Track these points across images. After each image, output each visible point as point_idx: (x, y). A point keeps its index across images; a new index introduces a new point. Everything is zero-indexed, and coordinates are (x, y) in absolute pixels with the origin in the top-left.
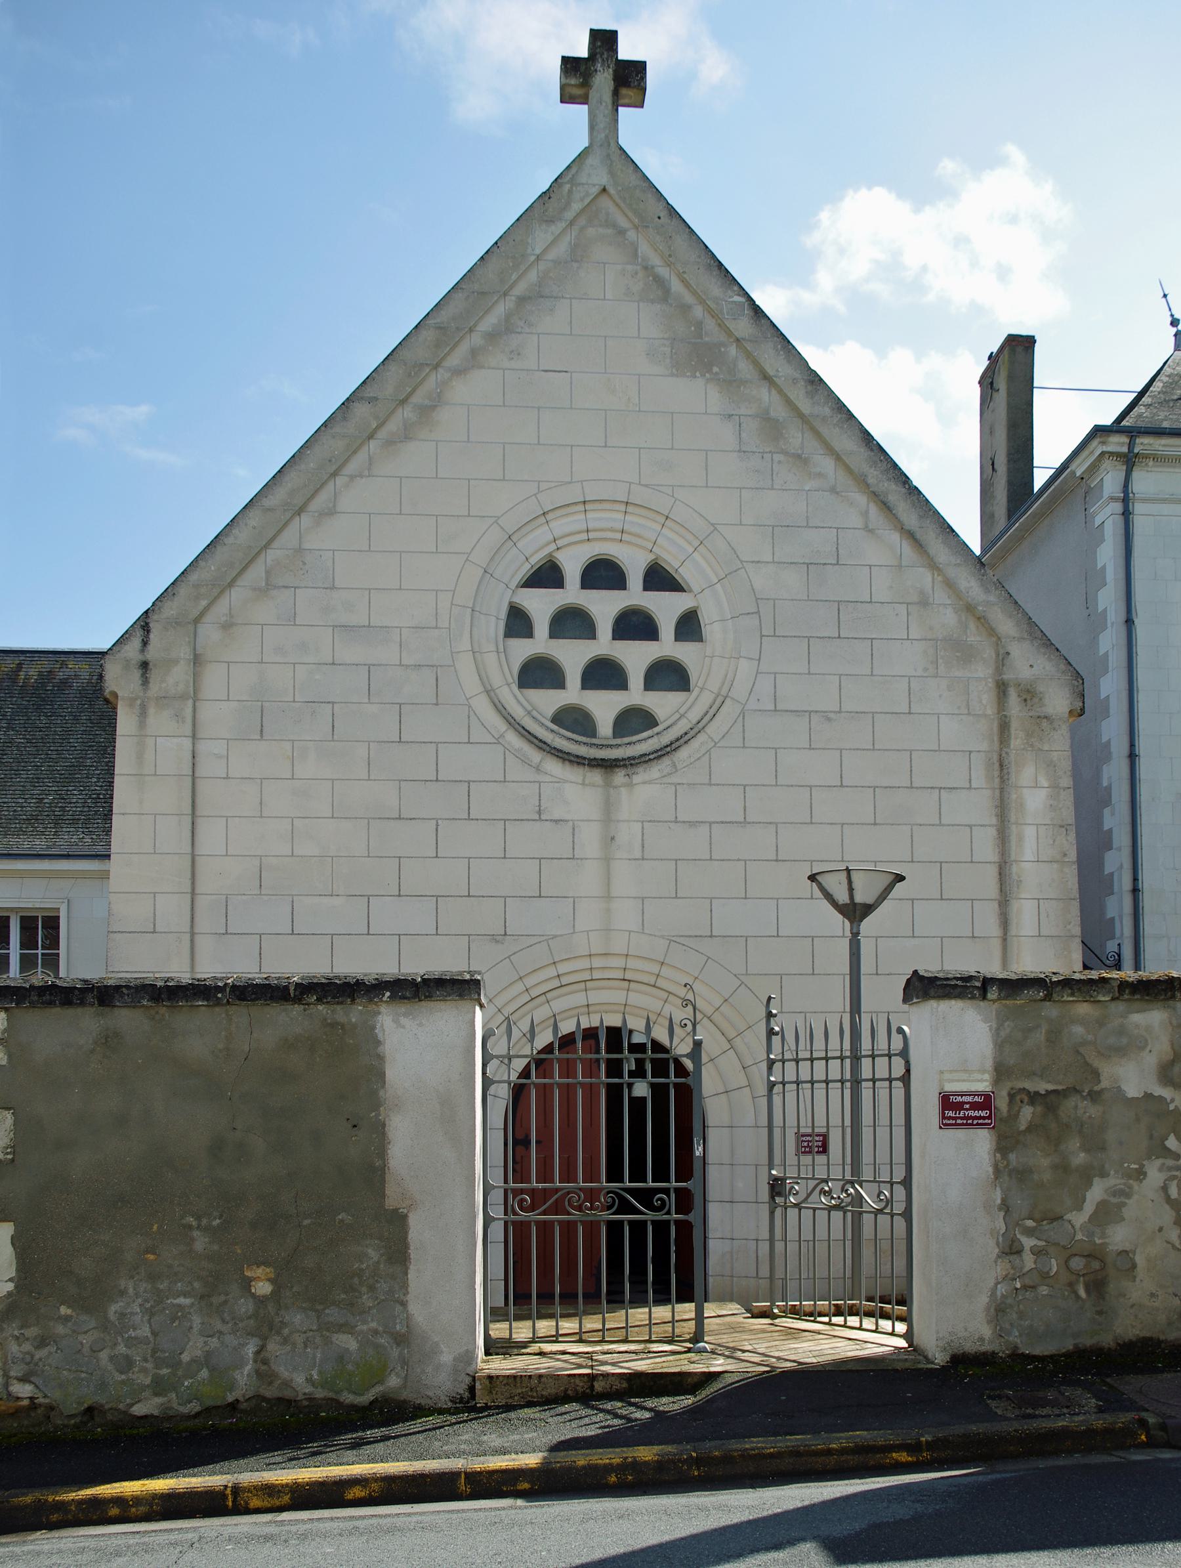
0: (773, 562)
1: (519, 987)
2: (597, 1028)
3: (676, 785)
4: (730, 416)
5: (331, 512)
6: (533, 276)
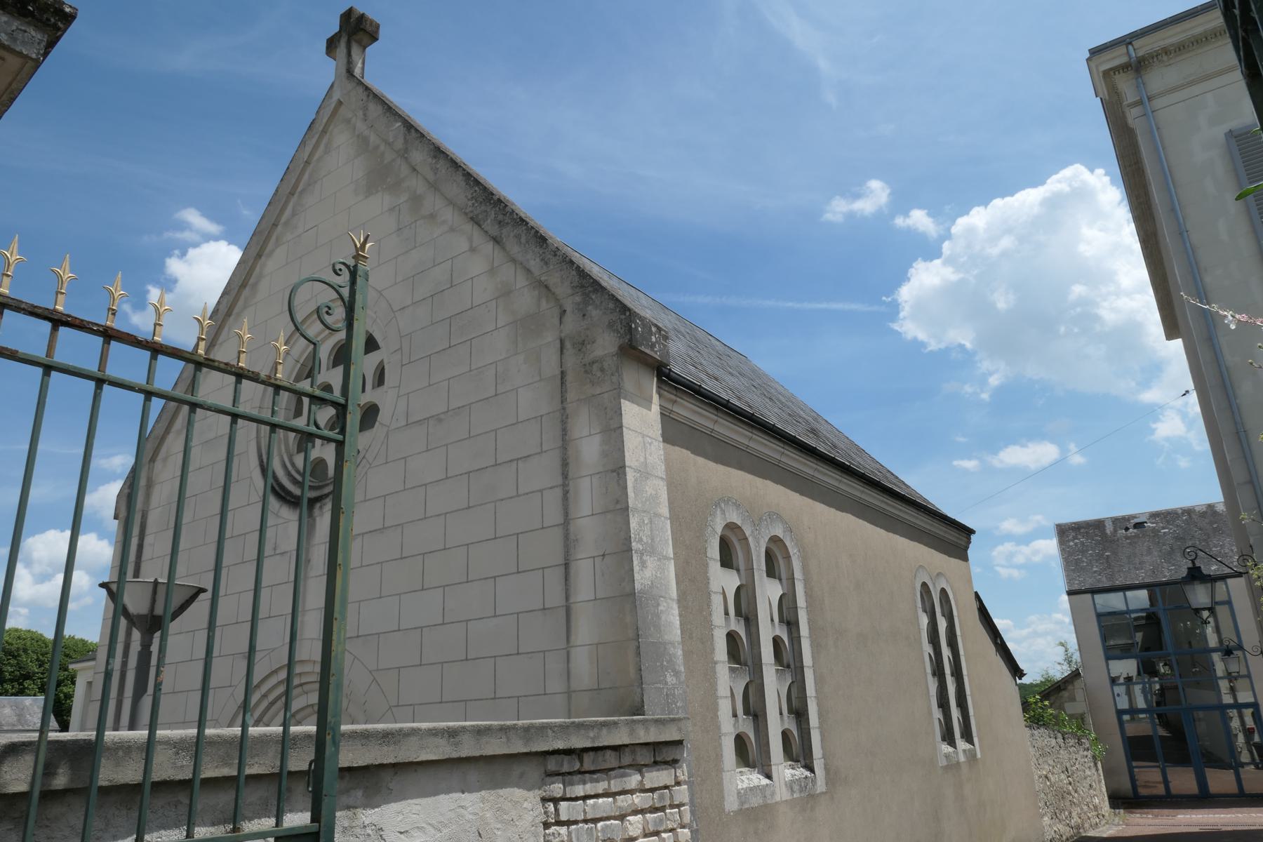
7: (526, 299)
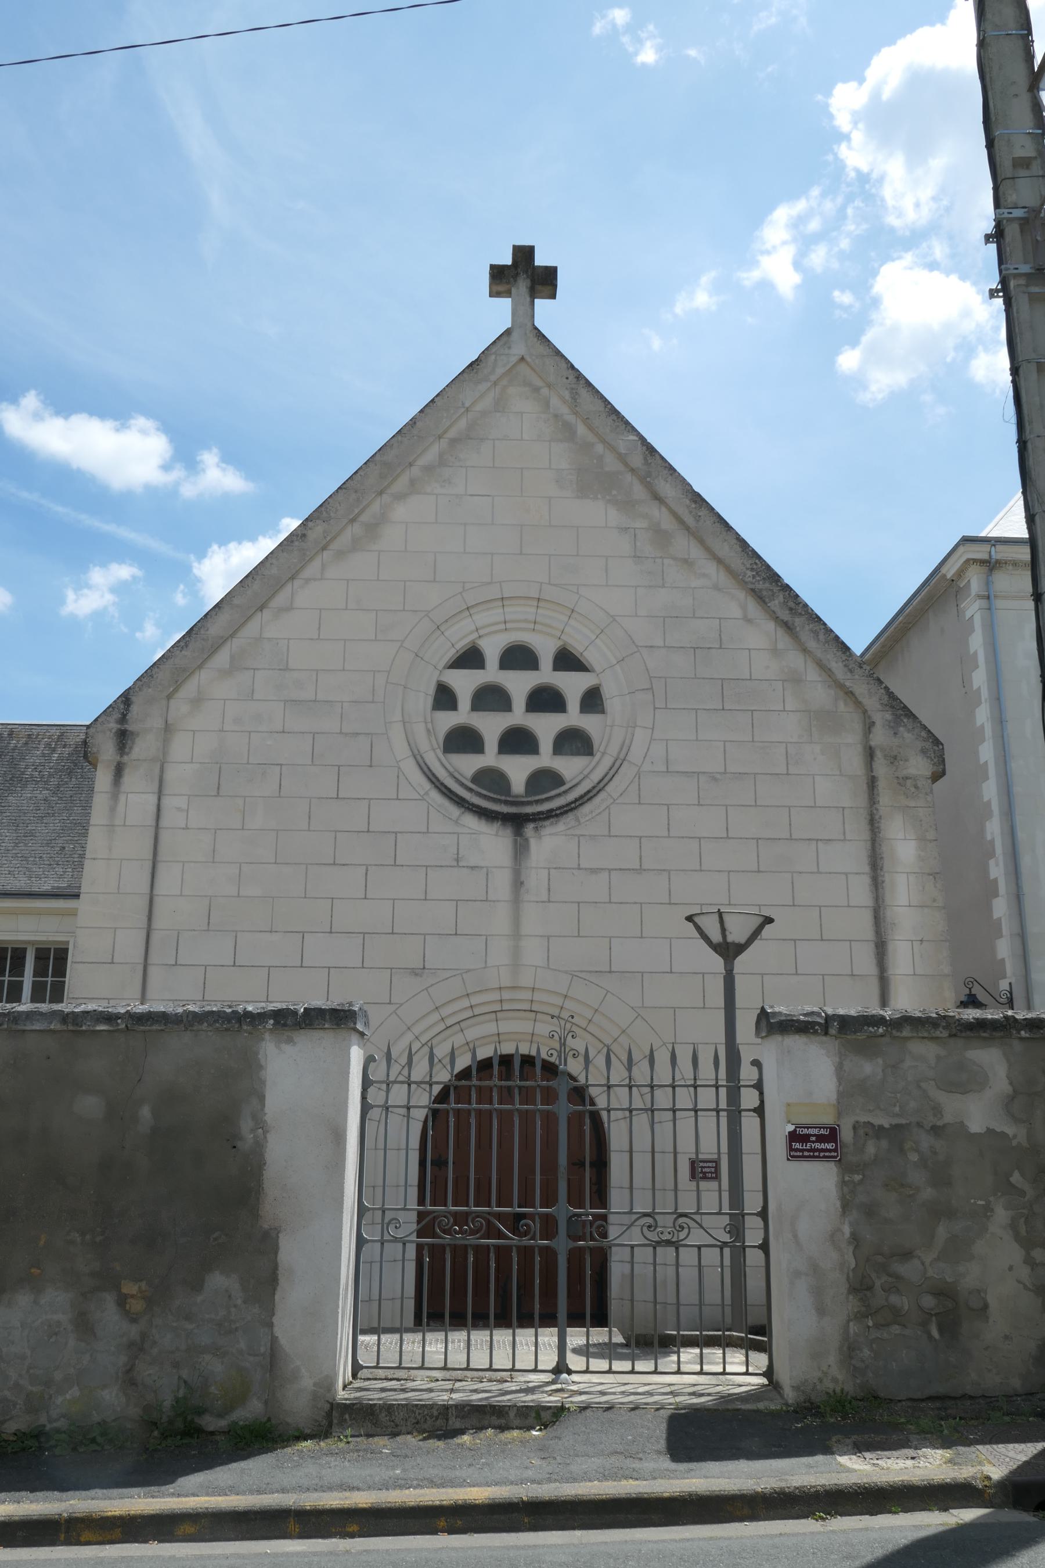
0: (665, 647)
1: (436, 1017)
2: (512, 1056)
3: (579, 836)
4: (627, 529)
5: (289, 608)
6: (463, 424)
7: (820, 694)
